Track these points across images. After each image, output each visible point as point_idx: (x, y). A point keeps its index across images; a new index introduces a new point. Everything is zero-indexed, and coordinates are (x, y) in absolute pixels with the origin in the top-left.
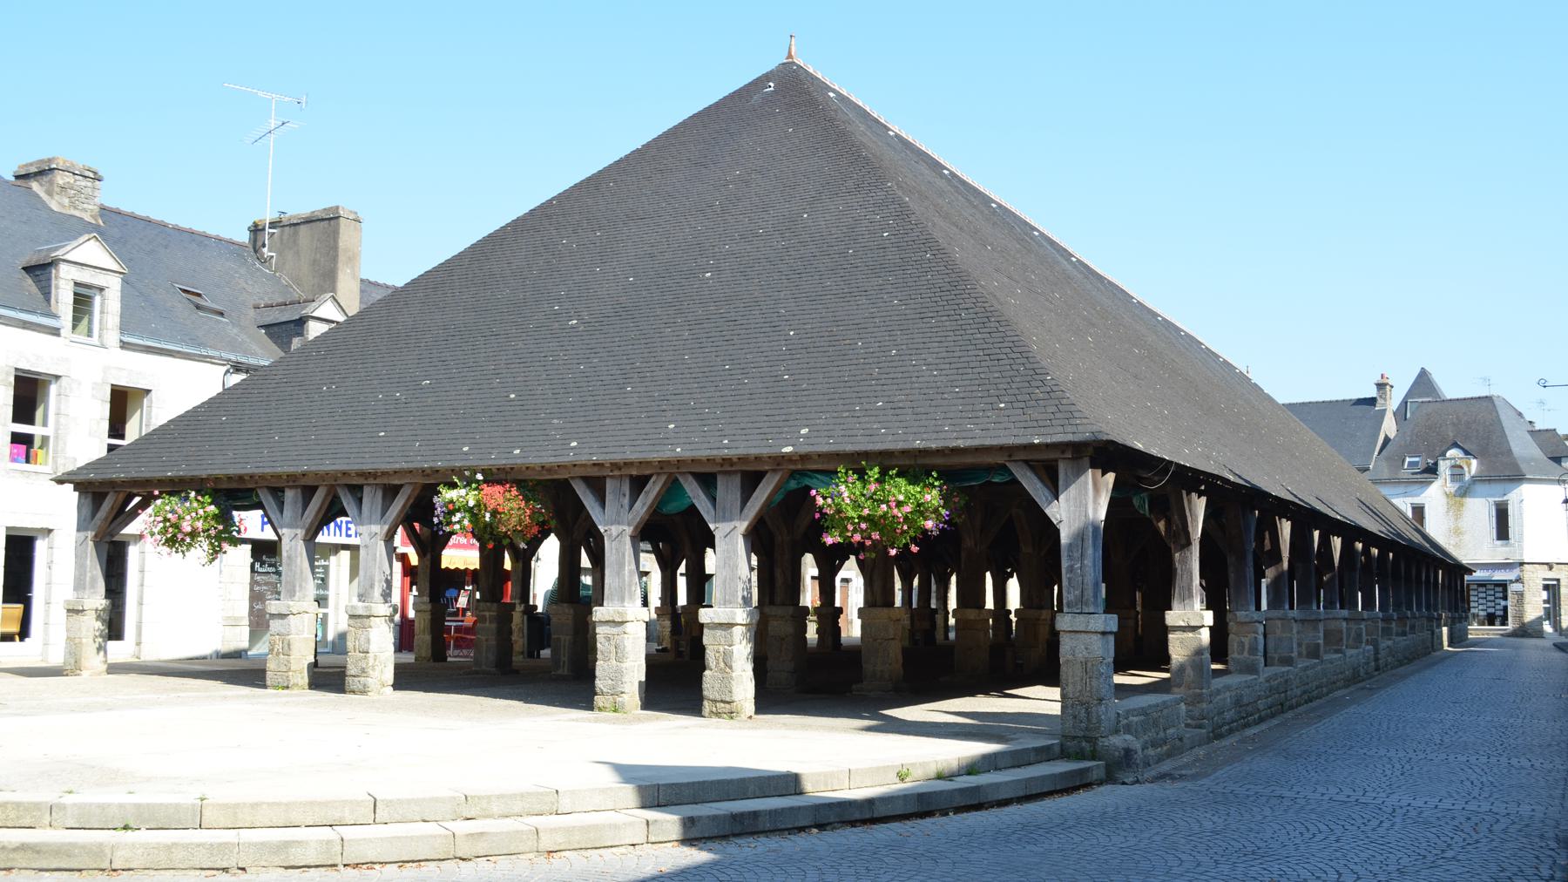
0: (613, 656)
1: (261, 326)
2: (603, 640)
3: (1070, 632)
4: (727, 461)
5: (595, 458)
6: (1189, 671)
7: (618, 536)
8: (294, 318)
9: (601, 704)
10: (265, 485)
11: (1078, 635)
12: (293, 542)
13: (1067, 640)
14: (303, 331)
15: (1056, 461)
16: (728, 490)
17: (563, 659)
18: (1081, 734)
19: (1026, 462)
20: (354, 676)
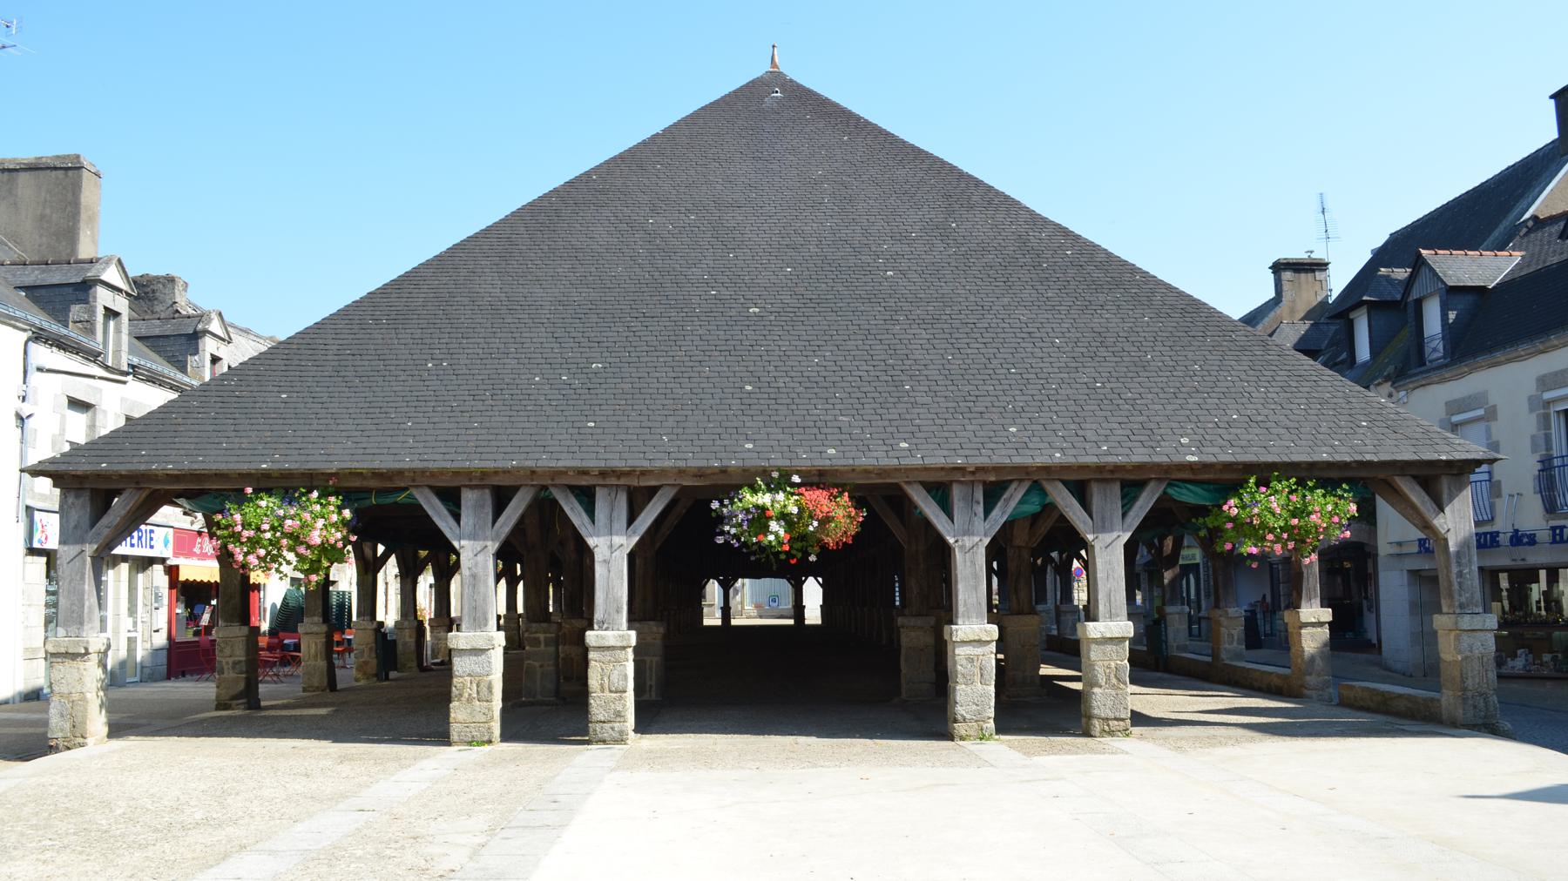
0: (977, 678)
1: (19, 287)
2: (964, 662)
3: (1469, 630)
4: (1100, 468)
5: (959, 461)
6: (1319, 661)
7: (973, 547)
8: (73, 281)
9: (963, 733)
10: (426, 484)
11: (1475, 633)
12: (480, 558)
13: (1465, 638)
14: (88, 296)
15: (951, 482)
16: (610, 506)
17: (648, 683)
18: (1480, 721)
19: (1415, 477)
20: (604, 722)
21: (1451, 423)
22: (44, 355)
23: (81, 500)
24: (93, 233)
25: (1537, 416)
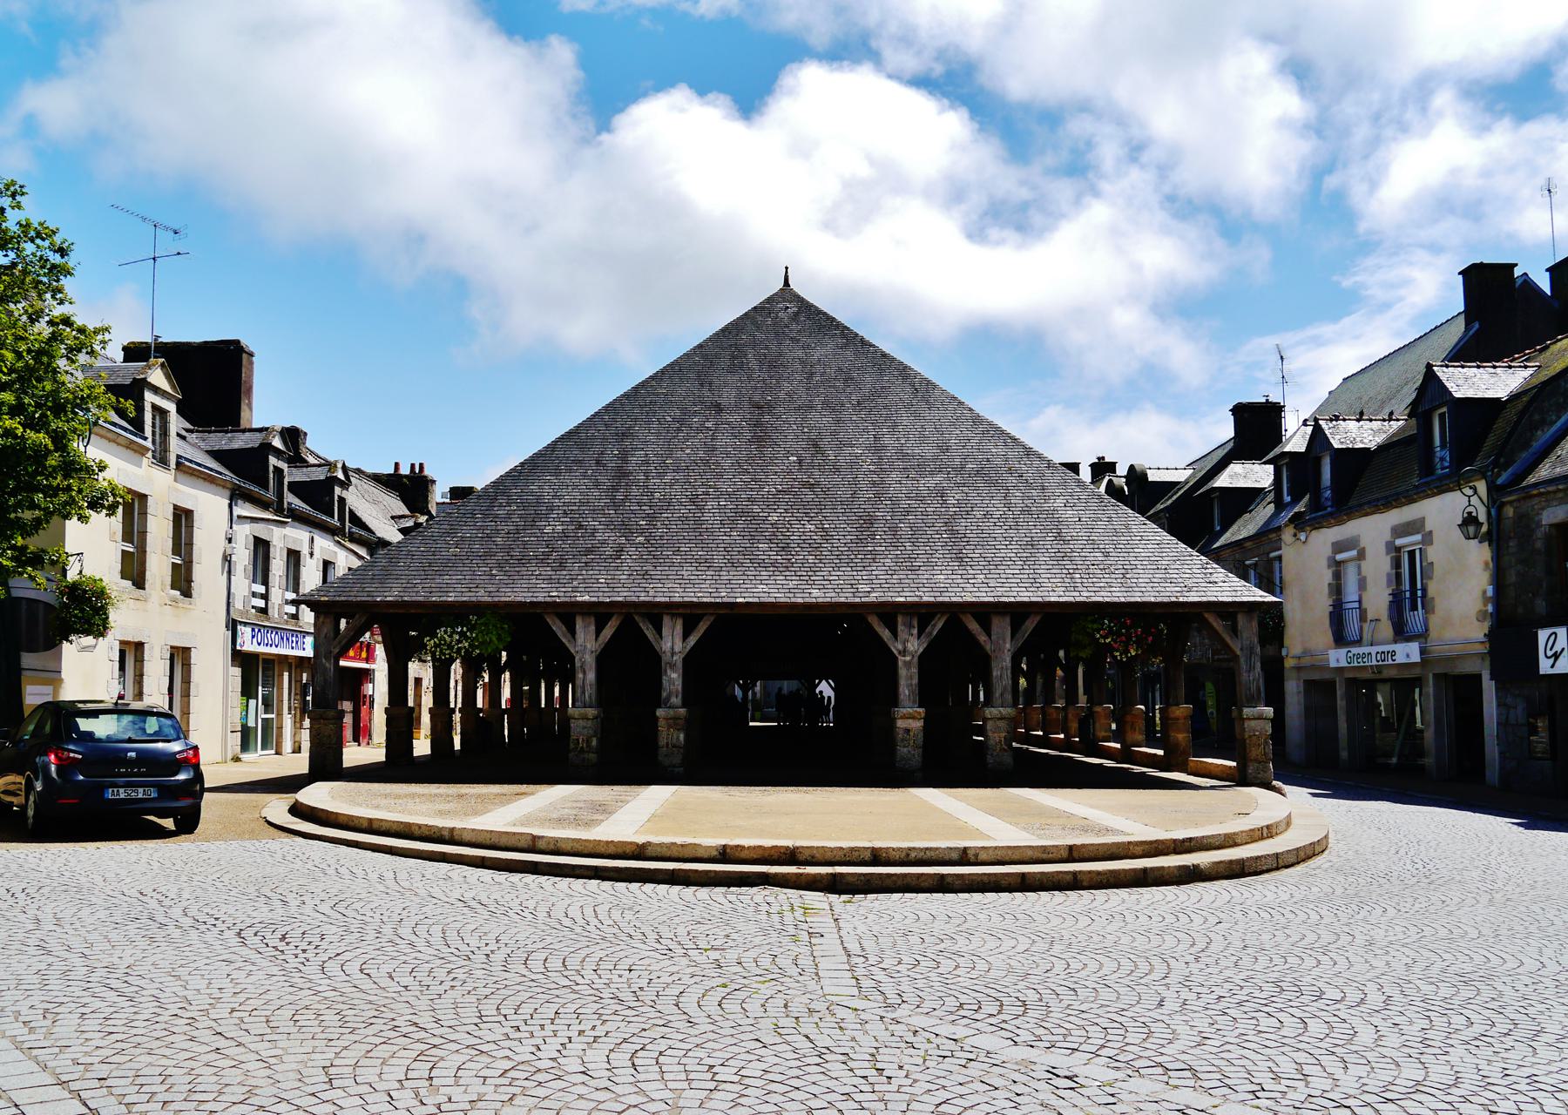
21: (1396, 547)
22: (244, 509)
23: (328, 620)
24: (249, 401)
25: (1392, 558)
